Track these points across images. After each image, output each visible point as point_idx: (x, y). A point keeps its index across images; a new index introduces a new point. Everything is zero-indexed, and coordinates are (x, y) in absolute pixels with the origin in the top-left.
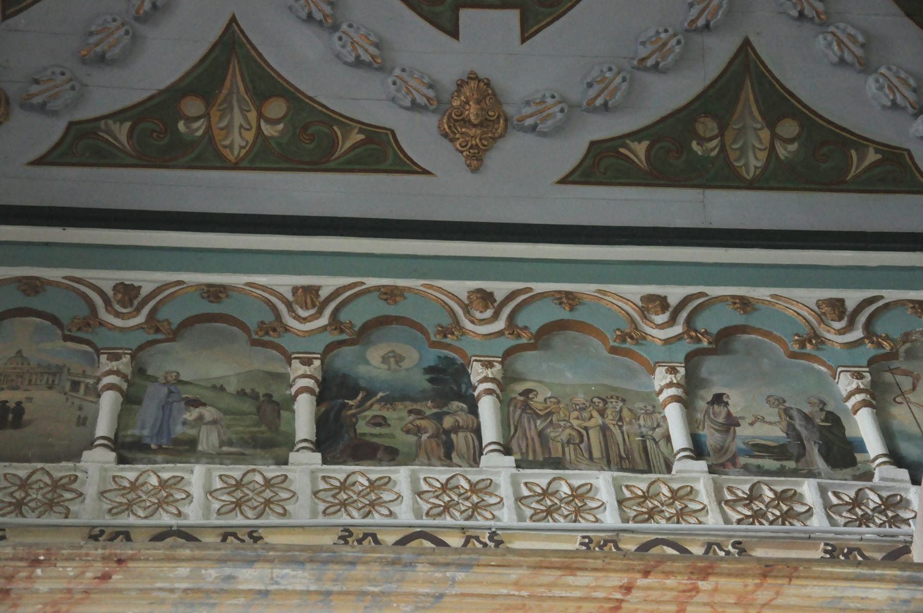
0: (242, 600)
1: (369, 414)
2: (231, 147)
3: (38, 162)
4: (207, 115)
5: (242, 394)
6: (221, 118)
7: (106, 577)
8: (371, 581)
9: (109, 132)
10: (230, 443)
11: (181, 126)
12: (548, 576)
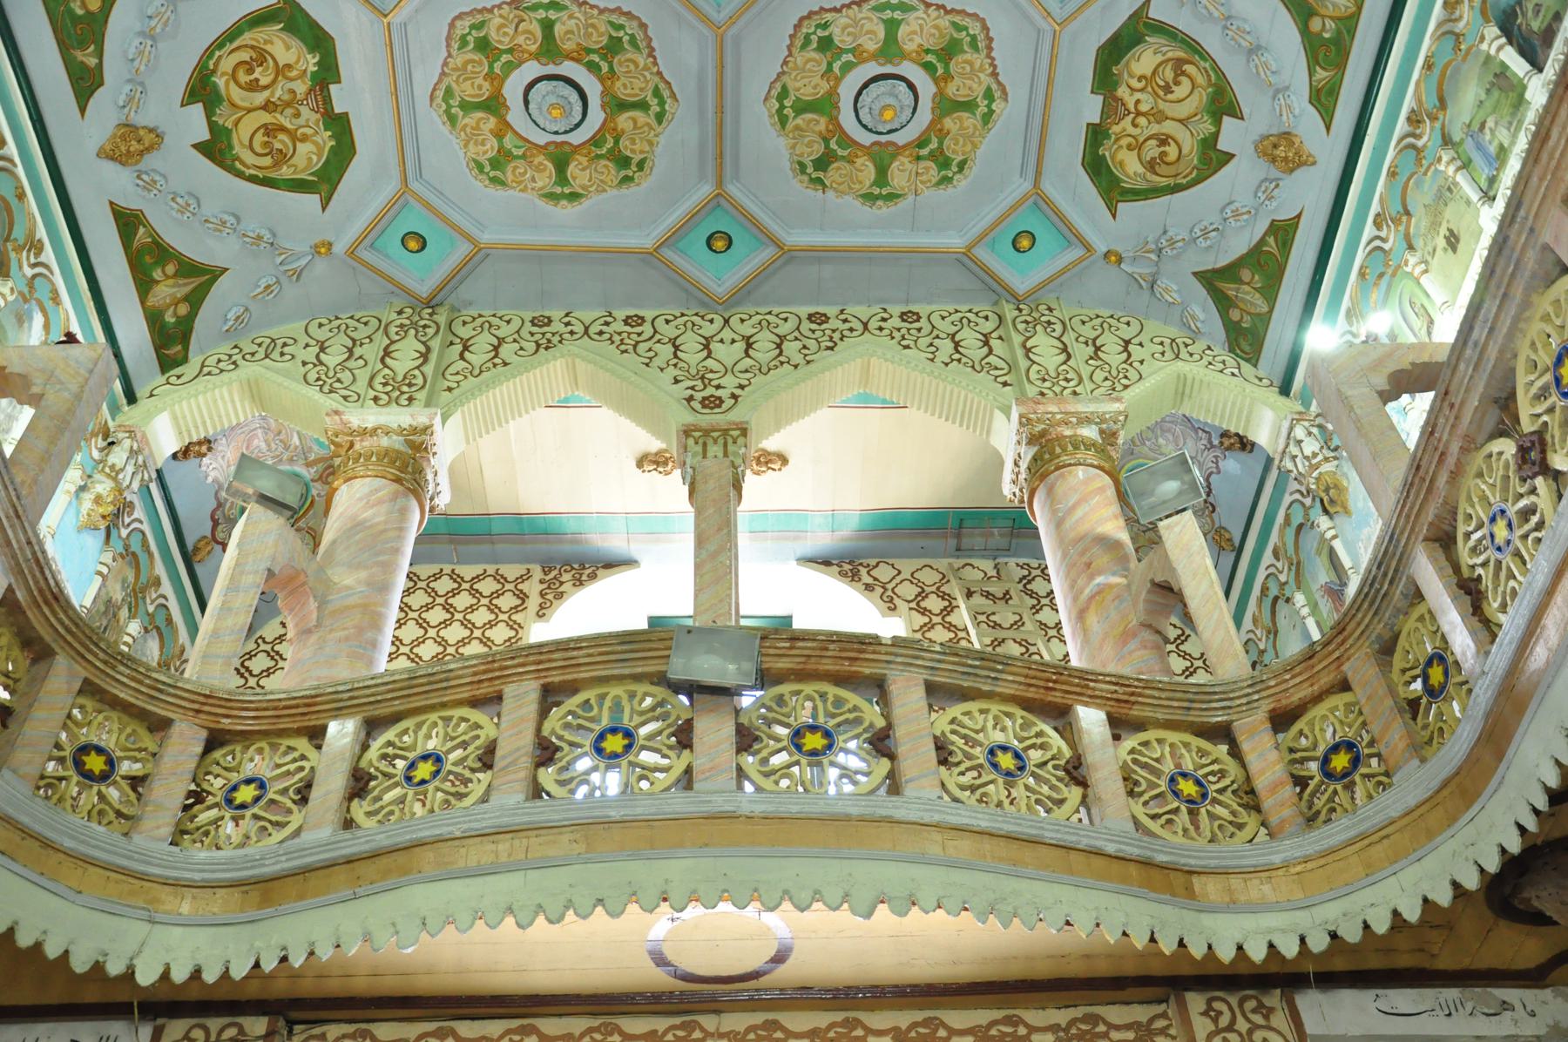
0: (1491, 343)
1: (1530, 14)
2: (1347, 7)
3: (1328, 128)
4: (1323, 17)
5: (1488, 91)
6: (1326, 7)
7: (1452, 406)
8: (1507, 266)
9: (1319, 81)
10: (1510, 123)
11: (1327, 35)
12: (1544, 156)
